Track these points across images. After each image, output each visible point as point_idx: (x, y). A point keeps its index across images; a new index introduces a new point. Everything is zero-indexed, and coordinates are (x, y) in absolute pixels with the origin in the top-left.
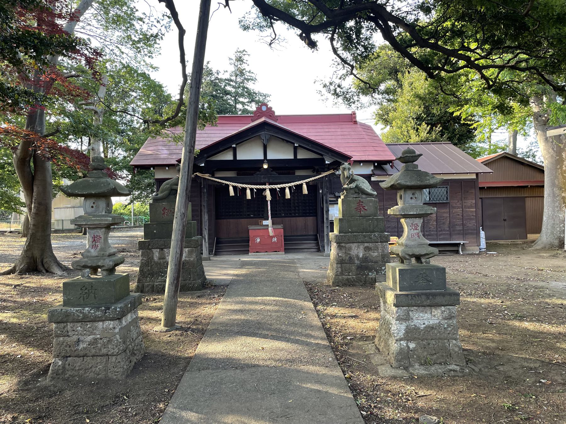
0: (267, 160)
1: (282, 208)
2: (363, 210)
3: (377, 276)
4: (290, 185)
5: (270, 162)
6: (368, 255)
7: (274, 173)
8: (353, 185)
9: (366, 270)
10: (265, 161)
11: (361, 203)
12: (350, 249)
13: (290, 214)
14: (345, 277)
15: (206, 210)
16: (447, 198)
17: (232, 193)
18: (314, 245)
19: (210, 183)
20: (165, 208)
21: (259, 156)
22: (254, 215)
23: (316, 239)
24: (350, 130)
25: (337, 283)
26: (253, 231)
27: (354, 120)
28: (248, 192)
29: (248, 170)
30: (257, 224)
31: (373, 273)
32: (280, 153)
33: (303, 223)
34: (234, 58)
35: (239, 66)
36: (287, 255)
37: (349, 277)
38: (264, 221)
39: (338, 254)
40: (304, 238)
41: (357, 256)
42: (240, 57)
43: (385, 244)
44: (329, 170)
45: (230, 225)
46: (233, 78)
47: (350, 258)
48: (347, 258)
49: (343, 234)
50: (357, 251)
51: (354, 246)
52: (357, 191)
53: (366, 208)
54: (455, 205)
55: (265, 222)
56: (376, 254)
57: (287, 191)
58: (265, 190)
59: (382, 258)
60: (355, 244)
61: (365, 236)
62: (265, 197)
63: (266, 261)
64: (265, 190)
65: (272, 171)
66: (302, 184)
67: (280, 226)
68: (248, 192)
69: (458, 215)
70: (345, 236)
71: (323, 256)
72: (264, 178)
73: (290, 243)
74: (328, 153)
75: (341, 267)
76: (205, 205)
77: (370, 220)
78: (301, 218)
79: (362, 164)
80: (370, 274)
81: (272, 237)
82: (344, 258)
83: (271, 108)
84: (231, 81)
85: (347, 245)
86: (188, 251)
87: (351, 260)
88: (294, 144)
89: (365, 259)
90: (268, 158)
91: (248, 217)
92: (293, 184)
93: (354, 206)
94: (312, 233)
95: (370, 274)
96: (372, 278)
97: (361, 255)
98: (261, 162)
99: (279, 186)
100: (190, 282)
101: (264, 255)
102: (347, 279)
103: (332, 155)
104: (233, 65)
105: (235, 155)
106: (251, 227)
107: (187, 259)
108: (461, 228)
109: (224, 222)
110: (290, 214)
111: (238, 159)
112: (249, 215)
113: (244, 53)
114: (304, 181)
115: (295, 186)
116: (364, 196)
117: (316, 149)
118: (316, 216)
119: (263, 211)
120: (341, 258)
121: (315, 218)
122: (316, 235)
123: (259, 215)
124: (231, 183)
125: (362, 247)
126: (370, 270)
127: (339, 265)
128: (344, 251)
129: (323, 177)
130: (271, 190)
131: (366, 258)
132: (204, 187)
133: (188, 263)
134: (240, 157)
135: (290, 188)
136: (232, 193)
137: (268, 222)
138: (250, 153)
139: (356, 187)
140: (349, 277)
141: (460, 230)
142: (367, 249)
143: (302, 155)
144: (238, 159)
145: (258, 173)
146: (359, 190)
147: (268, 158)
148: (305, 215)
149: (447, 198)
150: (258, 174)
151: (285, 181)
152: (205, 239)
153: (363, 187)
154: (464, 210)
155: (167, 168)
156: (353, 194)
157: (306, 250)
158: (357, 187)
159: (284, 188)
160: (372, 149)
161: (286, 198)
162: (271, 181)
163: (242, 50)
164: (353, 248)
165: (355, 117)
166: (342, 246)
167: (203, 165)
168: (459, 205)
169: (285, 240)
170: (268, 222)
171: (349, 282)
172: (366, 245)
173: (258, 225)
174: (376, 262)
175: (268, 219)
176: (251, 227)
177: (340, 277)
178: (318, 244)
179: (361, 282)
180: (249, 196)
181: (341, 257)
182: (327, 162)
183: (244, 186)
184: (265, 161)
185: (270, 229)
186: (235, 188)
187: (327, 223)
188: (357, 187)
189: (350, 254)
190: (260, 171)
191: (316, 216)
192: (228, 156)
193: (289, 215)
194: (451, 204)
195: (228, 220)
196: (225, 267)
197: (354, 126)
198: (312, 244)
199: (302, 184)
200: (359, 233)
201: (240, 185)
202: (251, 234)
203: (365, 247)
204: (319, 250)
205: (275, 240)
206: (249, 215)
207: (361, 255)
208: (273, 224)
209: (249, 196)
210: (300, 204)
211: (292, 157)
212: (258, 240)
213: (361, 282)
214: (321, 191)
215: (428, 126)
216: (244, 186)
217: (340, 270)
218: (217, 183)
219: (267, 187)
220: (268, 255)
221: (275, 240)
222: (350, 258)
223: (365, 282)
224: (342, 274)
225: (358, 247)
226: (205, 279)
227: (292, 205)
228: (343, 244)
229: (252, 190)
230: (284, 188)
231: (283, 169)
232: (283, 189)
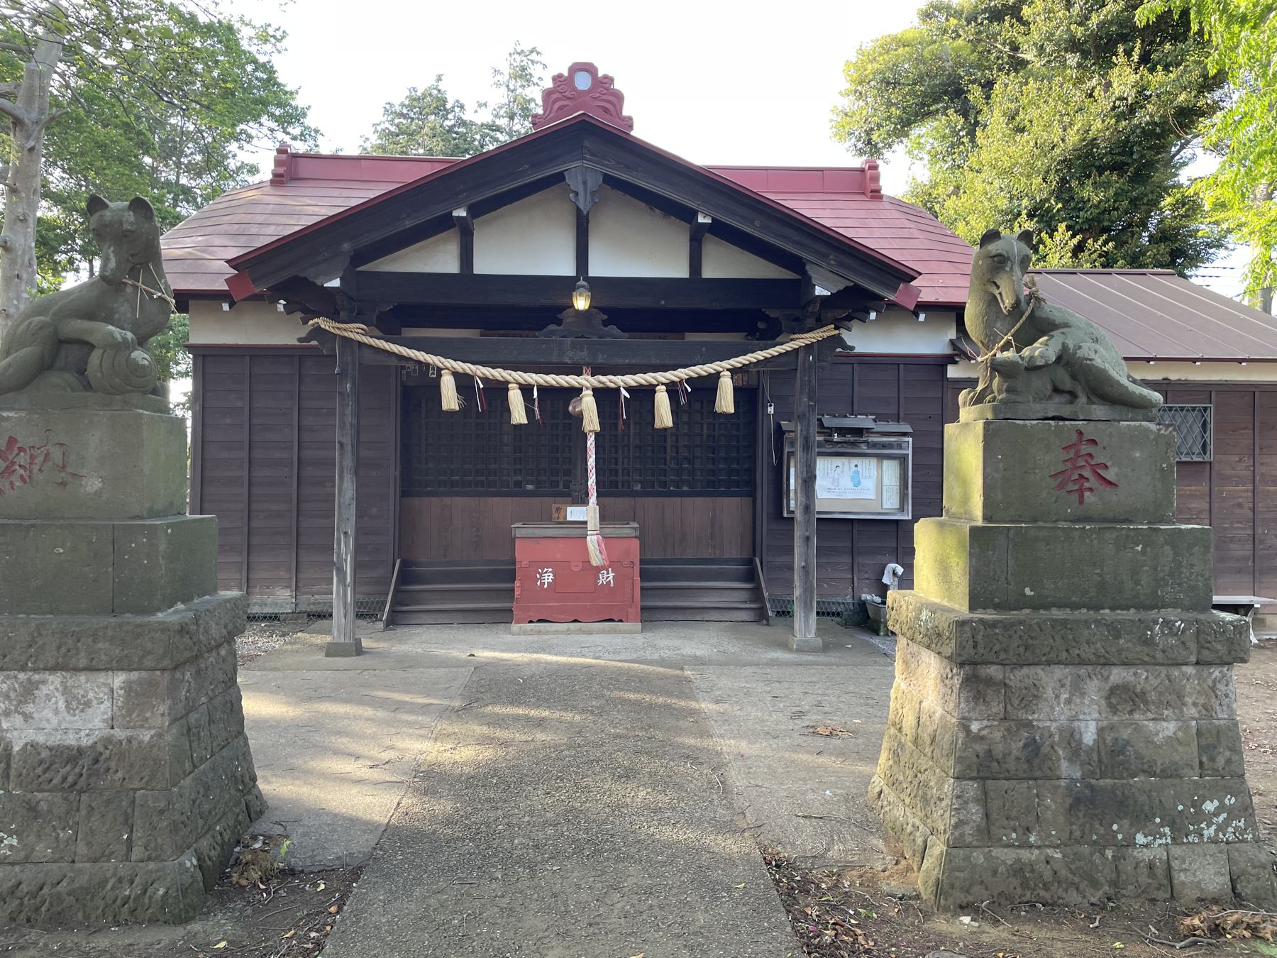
0: (587, 279)
1: (640, 463)
2: (1093, 482)
3: (1177, 851)
4: (671, 376)
5: (600, 286)
6: (1126, 734)
7: (613, 329)
8: (1041, 350)
9: (1118, 818)
10: (582, 282)
11: (1085, 449)
12: (1031, 696)
13: (664, 484)
14: (1007, 856)
15: (349, 462)
16: (1204, 446)
17: (450, 399)
18: (743, 595)
19: (368, 356)
20: (12, 441)
21: (555, 260)
22: (538, 484)
23: (751, 576)
24: (862, 214)
25: (957, 893)
26: (530, 542)
27: (873, 186)
28: (515, 397)
29: (518, 314)
30: (546, 518)
31: (1156, 834)
32: (639, 255)
33: (715, 518)
34: (506, 70)
35: (519, 91)
36: (649, 635)
37: (1025, 855)
38: (569, 509)
39: (964, 725)
40: (705, 568)
41: (1071, 737)
42: (523, 69)
43: (1216, 673)
44: (820, 323)
45: (452, 517)
46: (503, 122)
47: (1033, 748)
48: (1017, 746)
49: (990, 615)
50: (1075, 710)
51: (1051, 679)
52: (1067, 383)
53: (1110, 475)
54: (1229, 472)
55: (574, 513)
56: (1169, 728)
57: (662, 399)
58: (577, 391)
59: (1202, 750)
60: (1059, 672)
61: (1115, 631)
62: (579, 418)
63: (570, 673)
64: (577, 391)
65: (605, 323)
66: (717, 376)
67: (630, 529)
68: (515, 397)
69: (1240, 505)
70: (1007, 626)
71: (785, 646)
72: (574, 345)
73: (660, 590)
74: (825, 257)
75: (984, 799)
76: (347, 441)
77: (1138, 536)
78: (699, 501)
79: (922, 317)
80: (1140, 839)
81: (598, 569)
82: (999, 749)
83: (609, 80)
84: (498, 129)
85: (1017, 677)
86: (128, 687)
87: (1035, 759)
88: (694, 214)
89: (1112, 757)
90: (594, 271)
91: (517, 491)
92: (682, 373)
93: (1049, 460)
94: (735, 554)
95: (1140, 839)
96: (1151, 866)
97: (1089, 735)
98: (566, 285)
99: (631, 380)
100: (124, 869)
101: (568, 632)
102: (1018, 870)
103: (841, 264)
104: (504, 88)
105: (467, 257)
106: (520, 530)
107: (119, 734)
108: (1246, 550)
109: (431, 508)
110: (664, 484)
111: (476, 271)
112: (518, 484)
113: (534, 56)
114: (726, 364)
115: (690, 381)
116: (1100, 411)
117: (785, 237)
118: (752, 494)
119: (568, 473)
120: (980, 748)
121: (747, 500)
122: (750, 562)
123: (554, 484)
124: (450, 363)
125: (1094, 689)
126: (1141, 819)
127: (972, 788)
128: (997, 708)
129: (796, 351)
130: (599, 393)
131: (1118, 750)
132: (343, 374)
133: (122, 756)
134: (484, 265)
135: (672, 389)
136: (450, 399)
137: (586, 513)
138: (526, 249)
139: (1059, 359)
140: (1025, 855)
141: (1245, 559)
142: (1123, 699)
143: (724, 264)
144: (476, 271)
145: (552, 327)
146: (1074, 377)
147: (594, 271)
148: (712, 489)
149: (1204, 446)
150: (552, 333)
151: (654, 361)
152: (341, 572)
153: (1098, 362)
154: (1260, 488)
155: (226, 307)
156: (1040, 398)
157: (715, 615)
158: (1065, 359)
159: (650, 391)
160: (946, 268)
161: (658, 425)
162: (600, 359)
163: (527, 48)
164: (1049, 693)
165: (876, 179)
166: (989, 681)
167: (336, 283)
168: (1243, 471)
169: (644, 575)
170: (586, 513)
171: (1025, 885)
172: (1118, 675)
173: (549, 520)
174: (1171, 773)
175: (583, 501)
176: (520, 530)
177: (978, 857)
178: (756, 595)
179: (1095, 884)
180: (518, 415)
181: (979, 738)
182: (819, 291)
183: (498, 374)
184: (582, 282)
185: (593, 541)
186: (464, 383)
187: (808, 522)
188: (1065, 359)
189: (1029, 725)
190: (559, 323)
191: (752, 494)
192: (440, 259)
193: (659, 488)
194: (1216, 467)
195: (447, 500)
196: (398, 707)
197: (874, 205)
198: (734, 593)
199: (717, 376)
200: (1075, 607)
201: (481, 371)
202: (523, 554)
203: (1113, 691)
204: (761, 616)
205: (607, 577)
206: (518, 484)
207: (1089, 735)
208: (603, 518)
209: (518, 415)
210: (698, 452)
211: (682, 272)
212: (548, 578)
213: (1095, 884)
214: (771, 410)
215: (1073, 236)
216: (498, 374)
217: (975, 813)
218: (394, 362)
219: (586, 381)
220: (581, 632)
221: (607, 577)
222: (1033, 748)
223: (1114, 884)
224: (987, 833)
225: (1077, 688)
226: (252, 808)
227: (670, 453)
228: (994, 671)
229: (526, 390)
230: (650, 391)
231: (642, 316)
232: (646, 393)
